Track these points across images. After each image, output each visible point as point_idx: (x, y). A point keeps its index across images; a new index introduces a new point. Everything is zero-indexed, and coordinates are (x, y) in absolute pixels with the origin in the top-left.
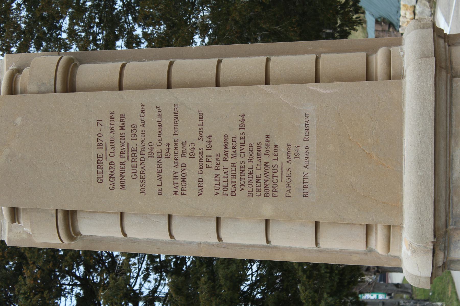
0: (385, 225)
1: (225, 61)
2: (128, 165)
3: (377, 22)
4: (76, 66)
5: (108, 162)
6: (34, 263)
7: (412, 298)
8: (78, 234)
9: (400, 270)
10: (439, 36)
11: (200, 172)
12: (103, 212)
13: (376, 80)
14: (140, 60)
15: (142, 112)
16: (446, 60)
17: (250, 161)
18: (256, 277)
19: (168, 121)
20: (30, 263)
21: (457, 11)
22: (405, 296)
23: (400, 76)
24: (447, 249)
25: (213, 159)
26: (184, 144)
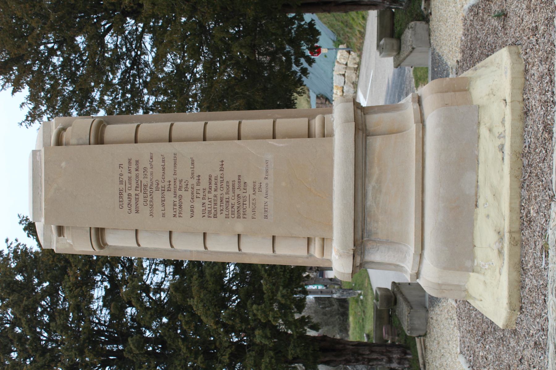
0: (320, 238)
1: (210, 123)
2: (141, 196)
3: (318, 97)
4: (104, 126)
5: (127, 194)
6: (75, 266)
7: (341, 288)
8: (105, 244)
9: (331, 269)
10: (358, 108)
11: (192, 201)
12: (124, 229)
13: (315, 137)
14: (150, 122)
15: (151, 158)
16: (362, 124)
17: (227, 193)
18: (233, 275)
19: (169, 165)
20: (73, 266)
21: (371, 91)
22: (336, 287)
23: (331, 135)
24: (362, 254)
25: (201, 192)
26: (181, 181)
